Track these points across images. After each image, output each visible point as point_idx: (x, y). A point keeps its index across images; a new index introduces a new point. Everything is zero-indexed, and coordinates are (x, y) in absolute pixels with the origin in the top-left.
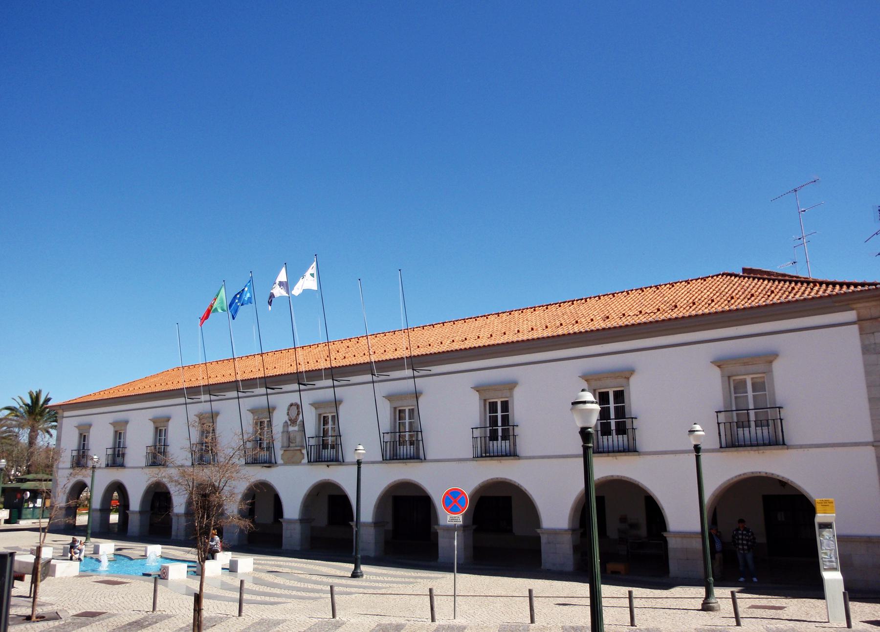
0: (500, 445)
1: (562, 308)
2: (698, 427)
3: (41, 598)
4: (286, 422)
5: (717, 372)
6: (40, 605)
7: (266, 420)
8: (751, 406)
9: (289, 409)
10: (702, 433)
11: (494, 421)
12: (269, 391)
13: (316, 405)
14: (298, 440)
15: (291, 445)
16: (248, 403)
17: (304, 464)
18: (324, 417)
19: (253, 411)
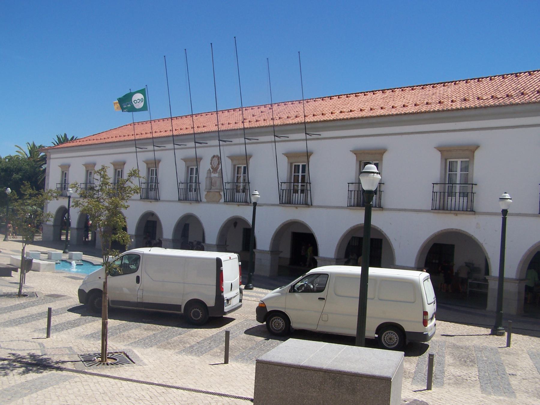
0: (298, 197)
1: (457, 87)
2: (507, 196)
3: (27, 283)
4: (209, 170)
5: (439, 154)
6: (25, 288)
7: (195, 168)
8: (458, 182)
9: (211, 161)
10: (259, 196)
11: (296, 180)
12: (156, 148)
13: (232, 158)
14: (218, 183)
15: (213, 188)
16: (181, 153)
17: (221, 203)
18: (238, 167)
19: (185, 160)
